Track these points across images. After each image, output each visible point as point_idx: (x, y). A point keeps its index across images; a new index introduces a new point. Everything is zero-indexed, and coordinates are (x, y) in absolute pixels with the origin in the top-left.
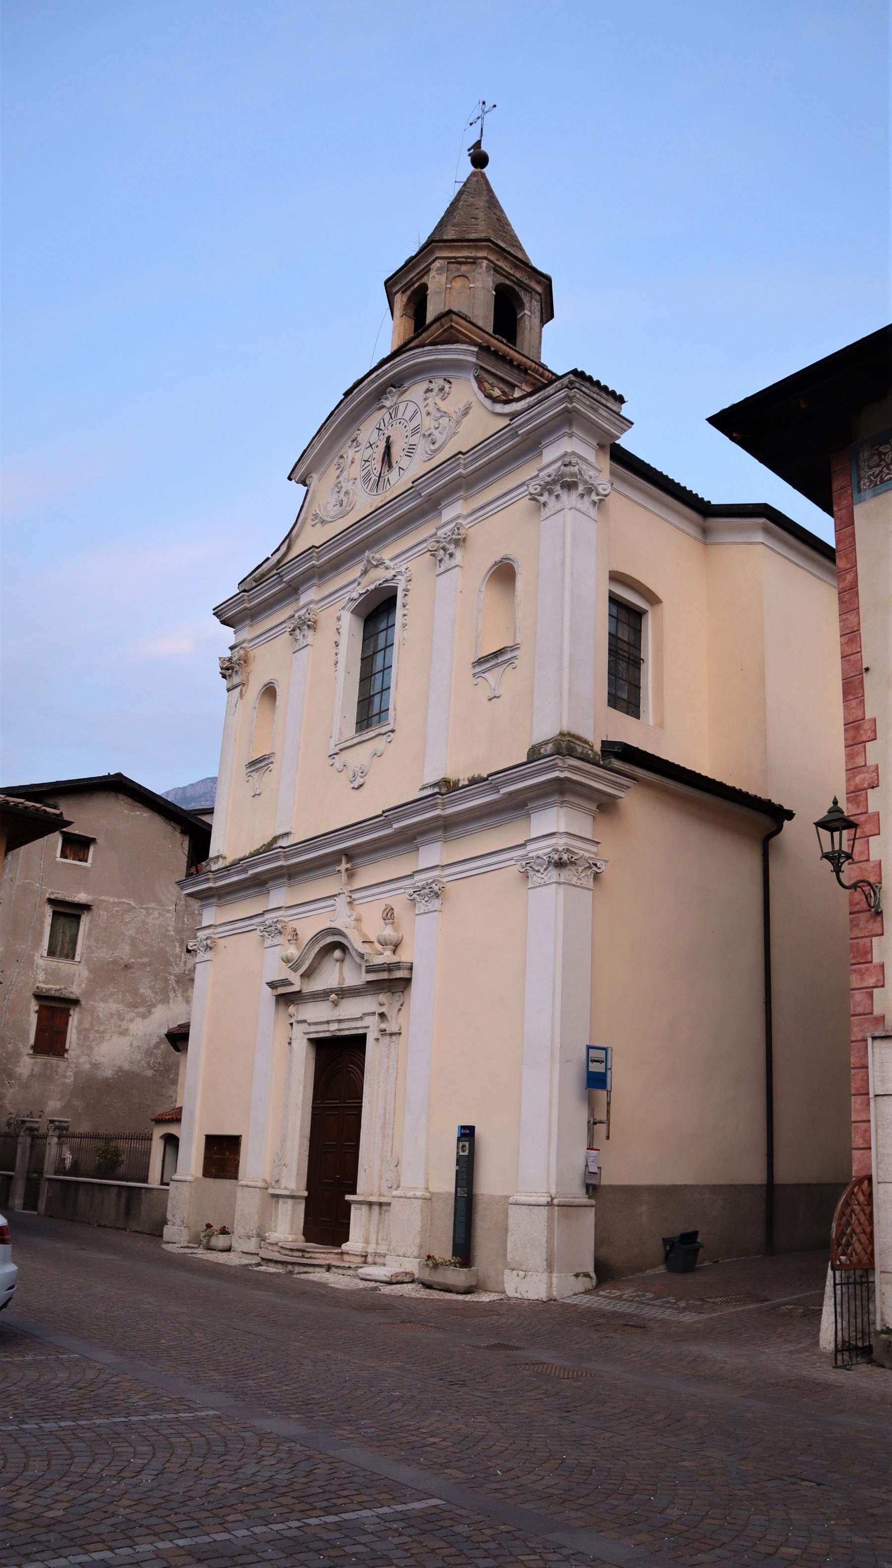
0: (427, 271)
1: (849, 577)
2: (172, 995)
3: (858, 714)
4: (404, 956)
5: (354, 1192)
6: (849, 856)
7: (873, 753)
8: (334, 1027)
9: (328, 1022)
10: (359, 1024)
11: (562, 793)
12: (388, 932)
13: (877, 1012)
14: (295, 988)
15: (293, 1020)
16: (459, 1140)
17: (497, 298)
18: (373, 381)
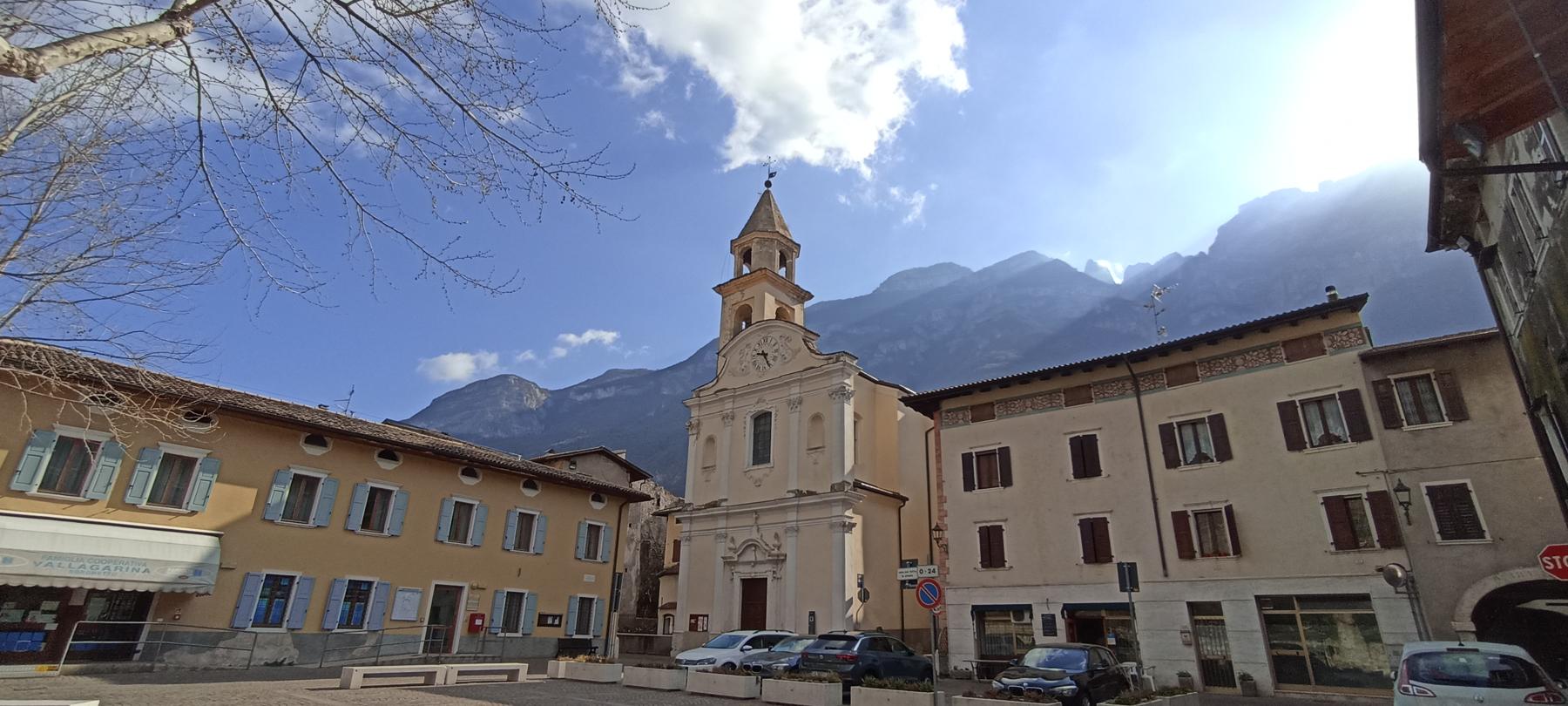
4: (783, 551)
7: (946, 506)
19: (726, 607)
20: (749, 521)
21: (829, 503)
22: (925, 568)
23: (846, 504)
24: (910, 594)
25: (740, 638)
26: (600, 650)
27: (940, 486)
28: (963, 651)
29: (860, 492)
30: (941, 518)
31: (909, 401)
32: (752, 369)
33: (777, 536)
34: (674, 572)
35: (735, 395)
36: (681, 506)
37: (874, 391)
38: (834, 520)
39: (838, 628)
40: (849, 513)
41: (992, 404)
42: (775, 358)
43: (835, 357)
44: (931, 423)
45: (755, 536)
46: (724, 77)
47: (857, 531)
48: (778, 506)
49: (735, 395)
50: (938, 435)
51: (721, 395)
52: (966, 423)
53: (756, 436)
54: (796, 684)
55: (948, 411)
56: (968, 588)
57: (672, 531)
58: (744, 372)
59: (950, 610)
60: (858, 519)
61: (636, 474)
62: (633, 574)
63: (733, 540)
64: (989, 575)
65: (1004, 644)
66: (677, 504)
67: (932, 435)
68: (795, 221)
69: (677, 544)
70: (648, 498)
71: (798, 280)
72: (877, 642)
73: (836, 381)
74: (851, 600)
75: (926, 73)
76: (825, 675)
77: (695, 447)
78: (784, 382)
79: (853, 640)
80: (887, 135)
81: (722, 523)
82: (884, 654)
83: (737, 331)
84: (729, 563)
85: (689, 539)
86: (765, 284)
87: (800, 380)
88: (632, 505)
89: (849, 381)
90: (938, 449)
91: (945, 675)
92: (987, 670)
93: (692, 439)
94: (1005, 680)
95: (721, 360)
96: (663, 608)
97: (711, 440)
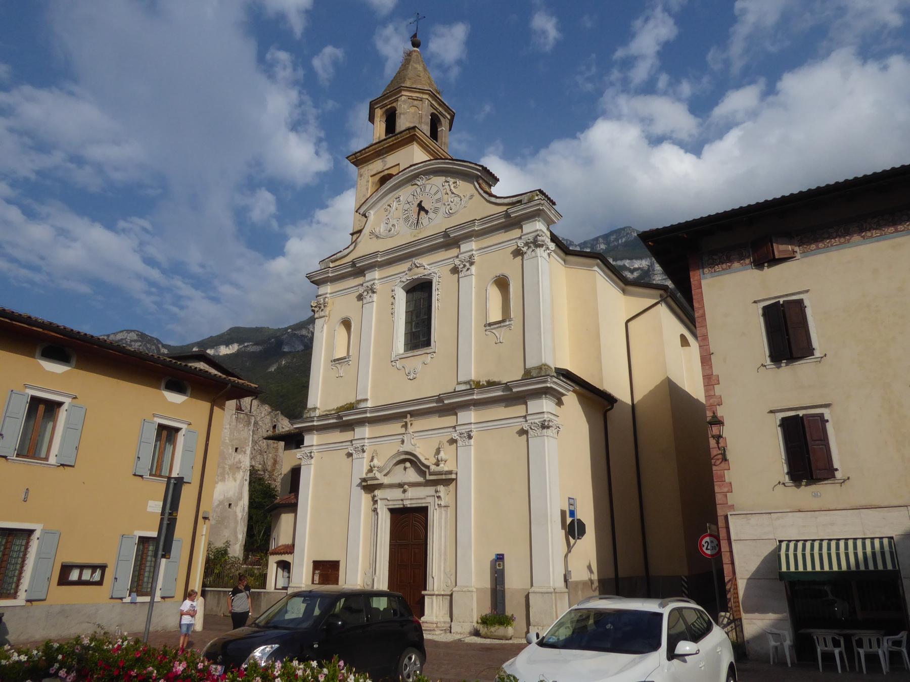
0: (396, 100)
2: (227, 476)
3: (709, 372)
5: (425, 590)
10: (423, 501)
11: (546, 394)
13: (730, 503)
17: (431, 120)
64: (806, 494)
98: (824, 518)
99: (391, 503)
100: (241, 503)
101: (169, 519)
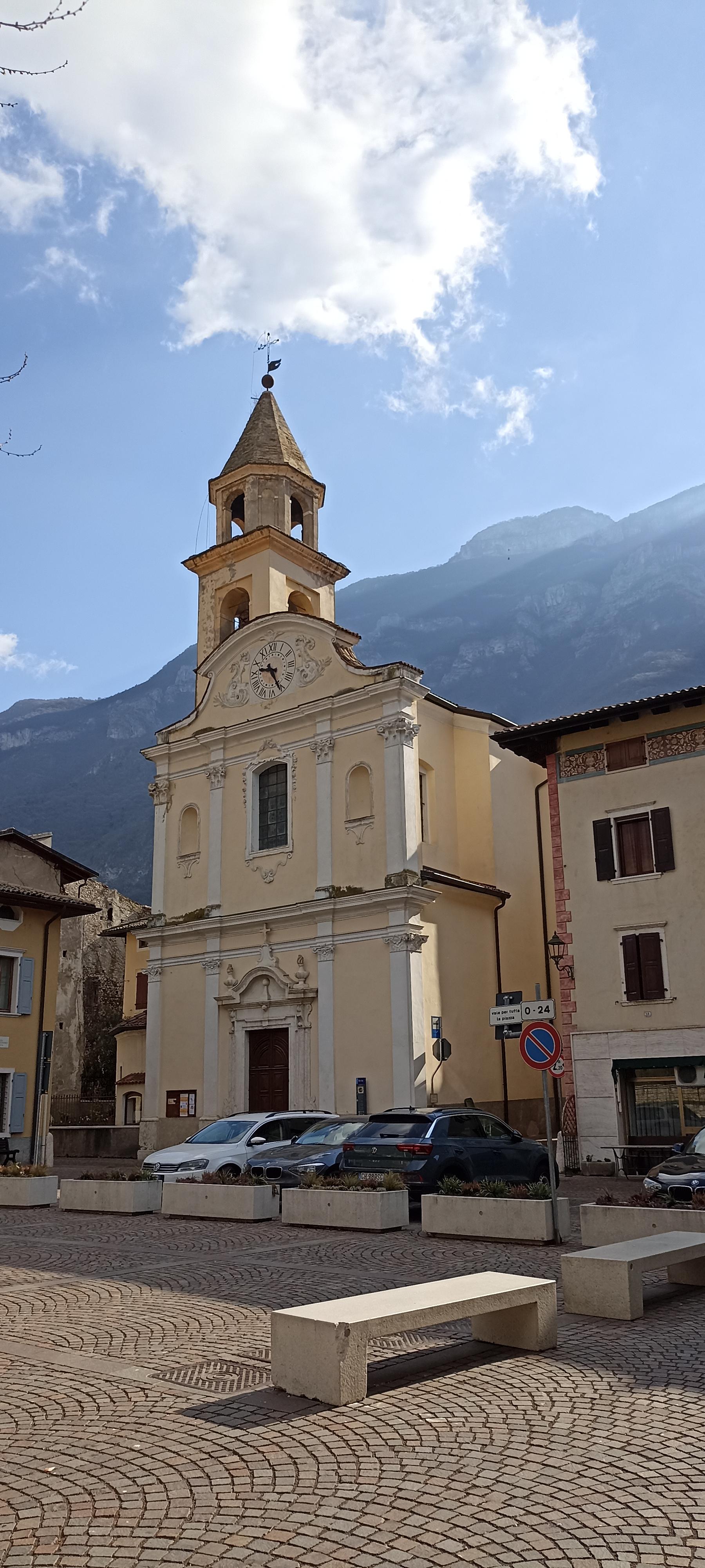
1: (556, 819)
3: (560, 886)
4: (312, 985)
6: (561, 957)
7: (569, 906)
8: (265, 1024)
9: (261, 1021)
10: (283, 1022)
12: (301, 971)
14: (237, 1001)
15: (234, 1020)
16: (357, 1086)
18: (258, 624)
19: (223, 1076)
20: (258, 938)
21: (383, 906)
22: (534, 1006)
23: (411, 905)
24: (513, 1045)
25: (246, 1125)
26: (23, 1155)
27: (559, 873)
28: (601, 1126)
29: (432, 887)
30: (561, 924)
31: (506, 740)
32: (252, 695)
33: (301, 961)
34: (139, 1026)
35: (228, 738)
36: (145, 919)
37: (452, 724)
38: (392, 932)
39: (401, 1103)
40: (415, 920)
41: (641, 740)
42: (289, 677)
43: (389, 671)
44: (543, 773)
45: (267, 962)
46: (171, 185)
47: (429, 949)
48: (303, 915)
49: (228, 738)
50: (554, 793)
51: (204, 738)
52: (599, 772)
53: (263, 803)
54: (335, 1194)
55: (570, 754)
56: (606, 1032)
57: (135, 959)
58: (241, 700)
59: (579, 1068)
60: (429, 930)
61: (71, 871)
62: (73, 1031)
63: (231, 970)
64: (639, 1012)
65: (666, 1118)
66: (140, 917)
67: (544, 792)
68: (314, 443)
69: (142, 980)
70: (90, 909)
71: (322, 547)
72: (462, 1123)
73: (388, 710)
74: (422, 1058)
75: (529, 162)
76: (380, 1178)
77: (165, 825)
78: (303, 716)
79: (424, 1121)
80: (454, 281)
81: (213, 944)
82: (473, 1141)
83: (226, 633)
84: (226, 1007)
85: (161, 972)
86: (268, 553)
87: (331, 711)
88: (66, 922)
89: (410, 710)
90: (555, 815)
91: (572, 1170)
92: (639, 1161)
93: (160, 811)
94: (663, 1176)
95: (202, 682)
96: (123, 1083)
97: (190, 811)
98: (653, 1037)
99: (249, 1025)
100: (75, 1022)
101: (44, 1064)
